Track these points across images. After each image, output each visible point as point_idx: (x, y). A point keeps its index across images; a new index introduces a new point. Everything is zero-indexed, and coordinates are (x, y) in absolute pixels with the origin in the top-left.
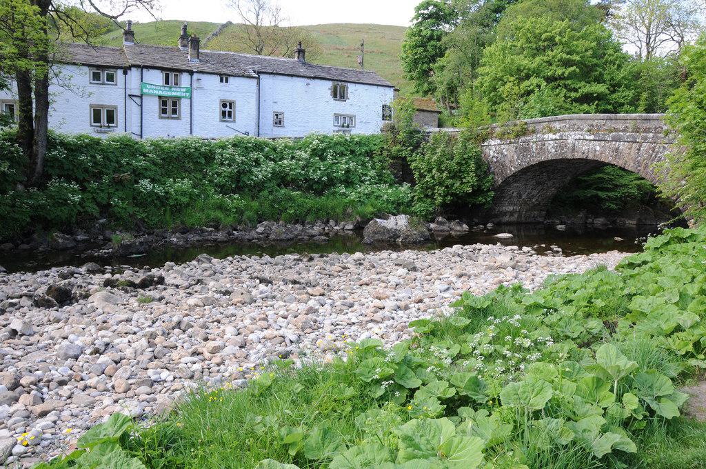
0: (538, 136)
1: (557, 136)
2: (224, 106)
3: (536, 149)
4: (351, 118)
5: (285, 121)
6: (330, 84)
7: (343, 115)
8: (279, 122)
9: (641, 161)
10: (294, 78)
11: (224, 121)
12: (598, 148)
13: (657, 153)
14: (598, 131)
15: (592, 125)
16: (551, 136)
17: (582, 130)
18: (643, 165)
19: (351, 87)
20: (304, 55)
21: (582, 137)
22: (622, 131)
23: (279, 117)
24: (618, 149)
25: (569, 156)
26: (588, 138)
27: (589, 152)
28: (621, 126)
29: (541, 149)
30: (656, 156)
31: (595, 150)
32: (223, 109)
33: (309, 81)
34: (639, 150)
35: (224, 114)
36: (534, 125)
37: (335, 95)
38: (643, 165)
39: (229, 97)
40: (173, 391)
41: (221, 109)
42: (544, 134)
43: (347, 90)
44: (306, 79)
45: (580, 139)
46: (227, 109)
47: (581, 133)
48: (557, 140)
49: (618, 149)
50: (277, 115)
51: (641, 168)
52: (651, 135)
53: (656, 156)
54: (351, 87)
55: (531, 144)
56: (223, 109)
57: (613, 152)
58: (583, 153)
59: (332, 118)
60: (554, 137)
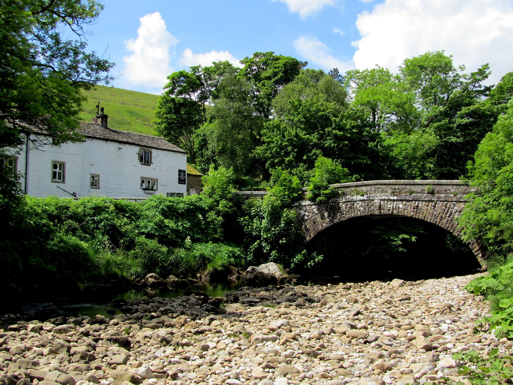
0: (347, 197)
1: (365, 198)
2: (55, 167)
3: (346, 208)
4: (155, 181)
5: (100, 183)
6: (137, 149)
7: (148, 178)
8: (95, 183)
9: (437, 215)
10: (109, 143)
11: (55, 182)
12: (401, 206)
13: (449, 208)
14: (400, 193)
15: (395, 189)
16: (359, 197)
17: (386, 192)
18: (439, 218)
19: (154, 152)
20: (106, 120)
21: (387, 198)
22: (419, 193)
23: (96, 179)
24: (418, 206)
25: (377, 213)
26: (392, 198)
27: (393, 209)
28: (419, 188)
29: (350, 208)
30: (448, 211)
31: (399, 208)
32: (54, 170)
33: (121, 146)
34: (435, 206)
35: (54, 174)
36: (343, 189)
37: (141, 159)
38: (439, 218)
39: (60, 159)
40: (460, 212)
41: (52, 170)
42: (352, 196)
43: (151, 155)
44: (118, 144)
45: (384, 200)
46: (58, 170)
47: (386, 194)
48: (365, 200)
49: (418, 206)
50: (93, 177)
51: (438, 220)
52: (443, 195)
53: (448, 211)
54: (154, 152)
55: (341, 204)
56: (54, 170)
57: (414, 209)
58: (389, 210)
59: (139, 182)
60: (362, 198)
